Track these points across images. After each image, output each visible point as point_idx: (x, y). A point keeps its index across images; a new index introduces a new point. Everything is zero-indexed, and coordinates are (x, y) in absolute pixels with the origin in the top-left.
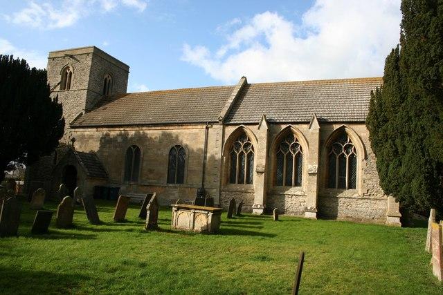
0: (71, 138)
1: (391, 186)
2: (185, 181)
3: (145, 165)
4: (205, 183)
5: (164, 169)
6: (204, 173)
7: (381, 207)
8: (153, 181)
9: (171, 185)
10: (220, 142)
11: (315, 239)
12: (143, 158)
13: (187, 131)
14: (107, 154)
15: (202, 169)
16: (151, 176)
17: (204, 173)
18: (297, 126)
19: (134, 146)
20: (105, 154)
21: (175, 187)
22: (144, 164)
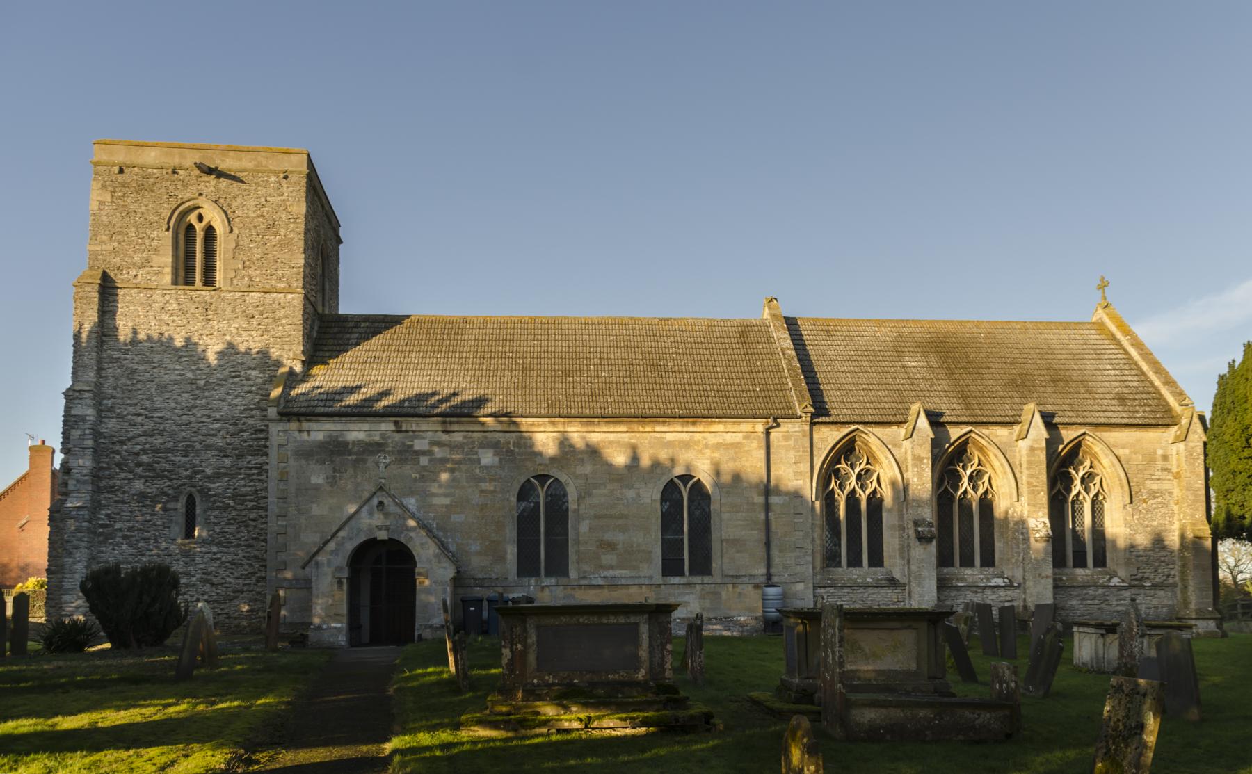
0: (170, 171)
1: (71, 393)
2: (715, 566)
3: (581, 529)
4: (773, 571)
5: (651, 540)
6: (768, 545)
7: (1166, 602)
8: (618, 573)
9: (676, 580)
10: (805, 467)
11: (262, 420)
12: (576, 511)
13: (712, 439)
14: (447, 501)
15: (763, 538)
16: (608, 558)
17: (768, 545)
18: (985, 431)
19: (542, 478)
20: (436, 501)
21: (689, 585)
22: (584, 527)
